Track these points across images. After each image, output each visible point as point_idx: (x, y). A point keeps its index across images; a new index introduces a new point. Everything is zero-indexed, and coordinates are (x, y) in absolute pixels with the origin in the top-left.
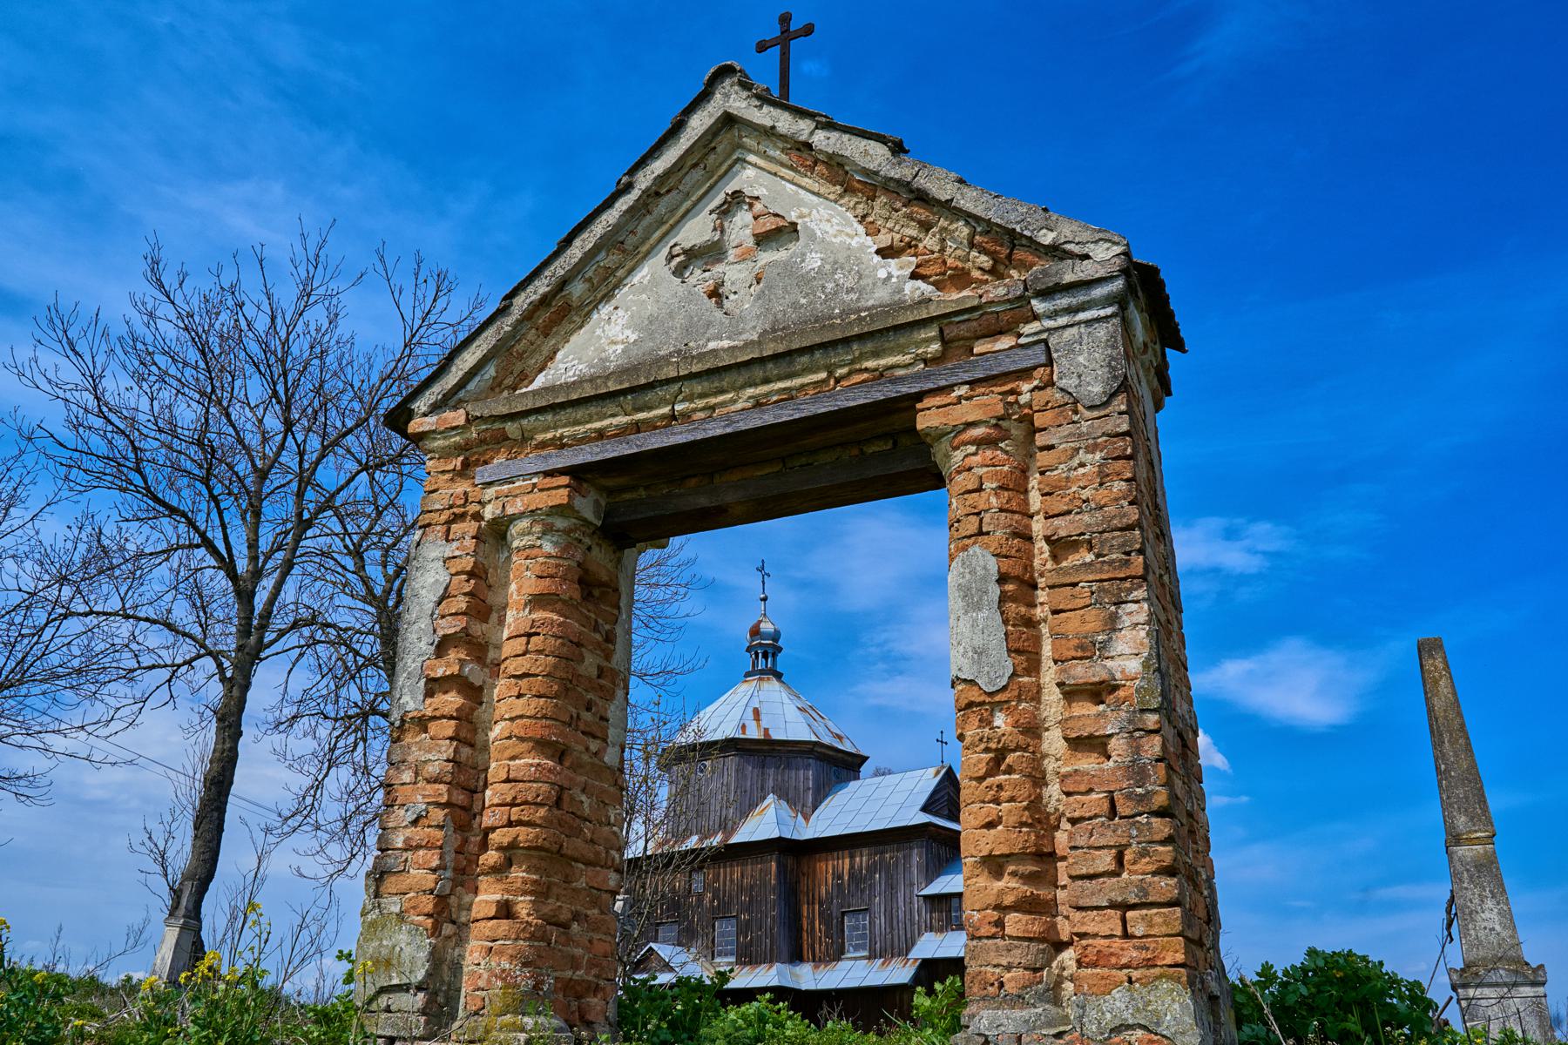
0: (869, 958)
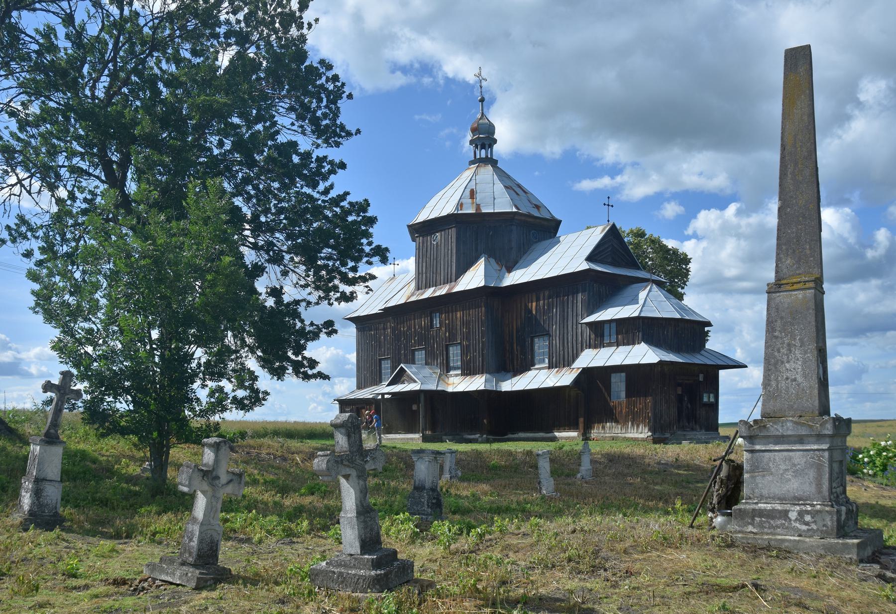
0: (549, 368)
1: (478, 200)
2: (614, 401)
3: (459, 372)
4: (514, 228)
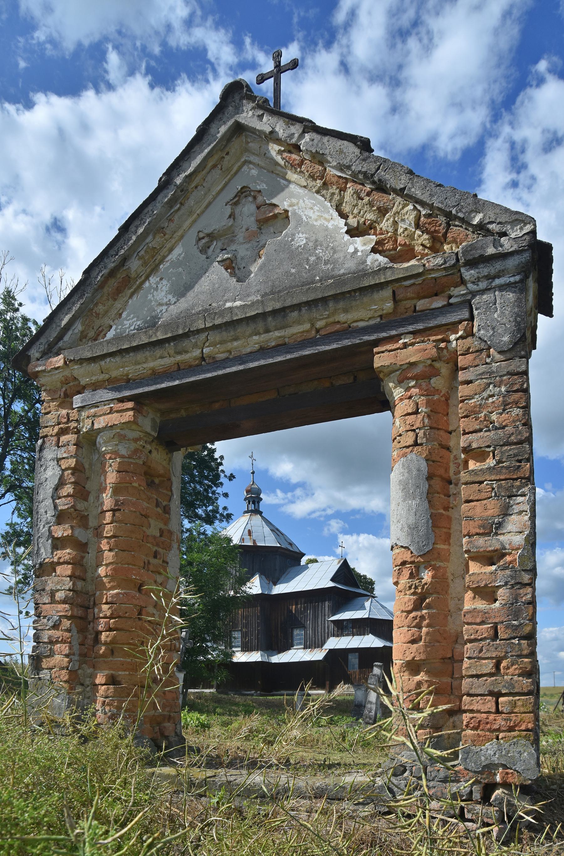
0: (304, 648)
2: (350, 671)
3: (240, 649)
4: (278, 556)
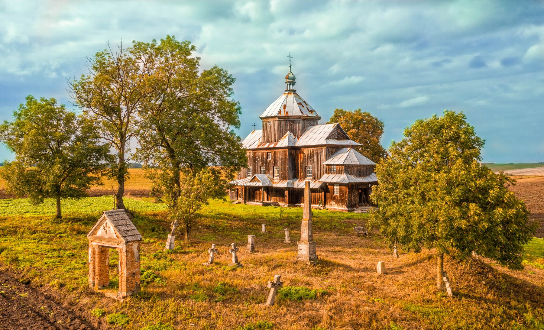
1: (287, 110)
